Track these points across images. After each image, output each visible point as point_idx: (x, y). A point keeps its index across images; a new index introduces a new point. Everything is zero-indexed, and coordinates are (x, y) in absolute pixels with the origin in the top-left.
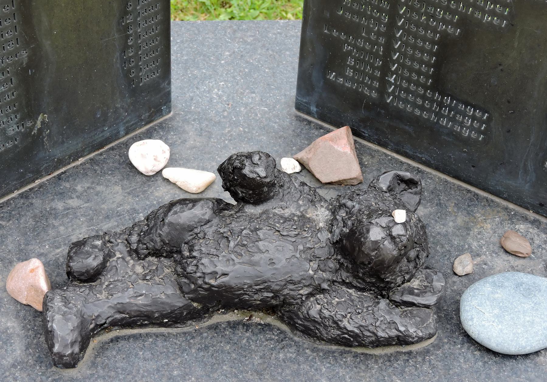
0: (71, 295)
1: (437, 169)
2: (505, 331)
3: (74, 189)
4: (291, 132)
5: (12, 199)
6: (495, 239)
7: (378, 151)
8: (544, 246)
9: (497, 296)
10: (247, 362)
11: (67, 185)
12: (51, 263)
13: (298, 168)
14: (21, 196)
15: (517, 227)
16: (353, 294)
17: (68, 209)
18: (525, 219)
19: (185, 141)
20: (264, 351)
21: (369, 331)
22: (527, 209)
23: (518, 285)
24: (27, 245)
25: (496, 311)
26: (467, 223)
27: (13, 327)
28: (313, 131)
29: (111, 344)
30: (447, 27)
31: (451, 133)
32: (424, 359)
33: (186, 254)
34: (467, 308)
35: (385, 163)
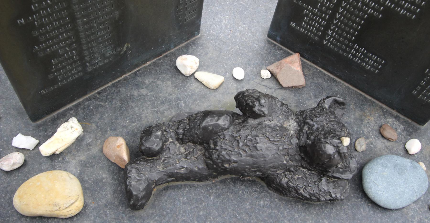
0: (142, 168)
1: (345, 81)
2: (390, 198)
3: (144, 83)
4: (265, 51)
5: (108, 87)
6: (377, 128)
7: (312, 66)
8: (402, 133)
9: (384, 173)
10: (242, 207)
11: (140, 79)
12: (130, 132)
13: (270, 76)
14: (114, 85)
15: (388, 120)
16: (306, 172)
17: (141, 96)
18: (392, 115)
19: (206, 54)
20: (252, 199)
21: (315, 196)
22: (394, 109)
23: (395, 166)
24: (116, 119)
25: (385, 185)
26: (361, 116)
27: (106, 178)
28: (277, 51)
29: (164, 192)
30: (374, 12)
31: (359, 66)
32: (341, 208)
33: (212, 146)
34: (368, 180)
35: (316, 74)
